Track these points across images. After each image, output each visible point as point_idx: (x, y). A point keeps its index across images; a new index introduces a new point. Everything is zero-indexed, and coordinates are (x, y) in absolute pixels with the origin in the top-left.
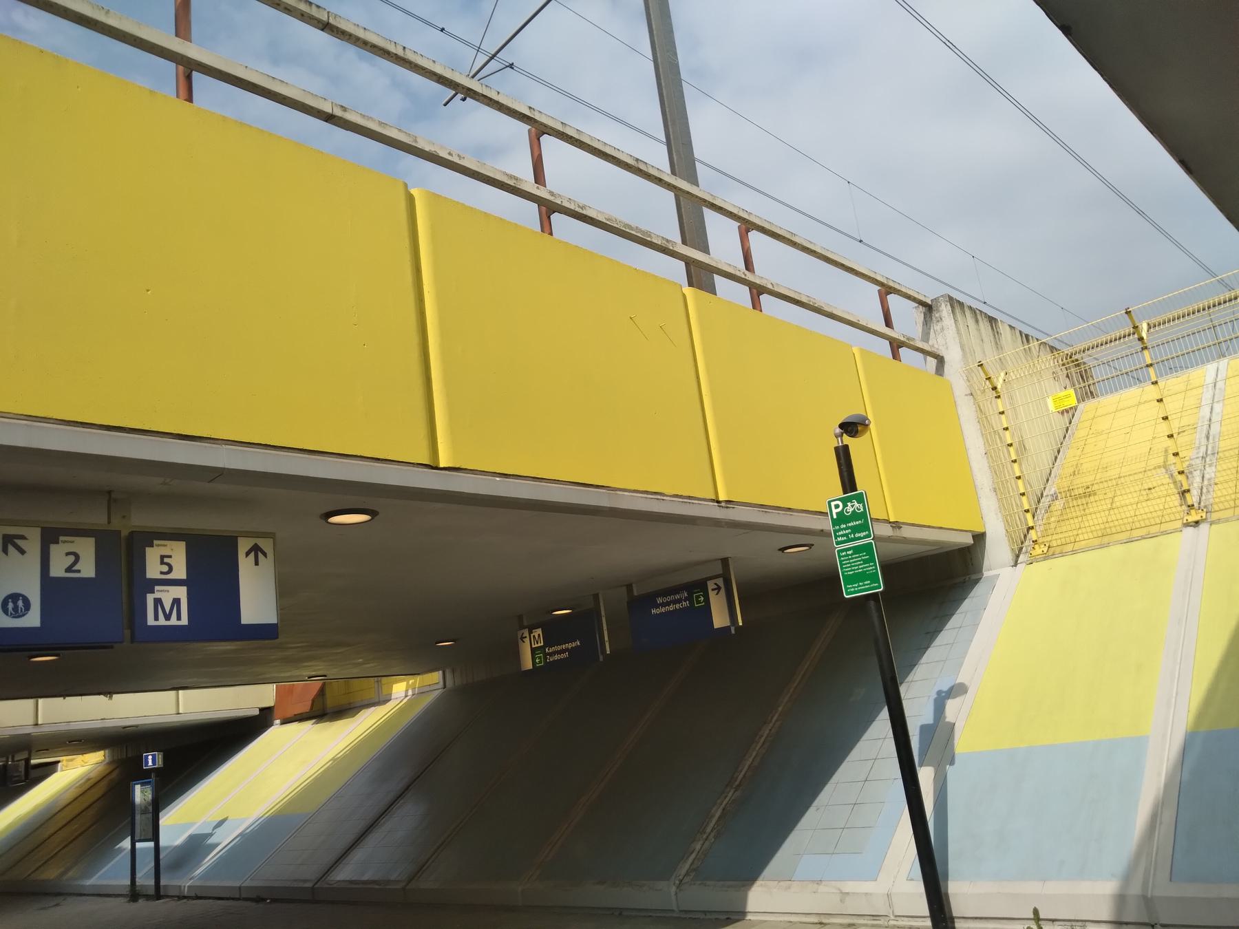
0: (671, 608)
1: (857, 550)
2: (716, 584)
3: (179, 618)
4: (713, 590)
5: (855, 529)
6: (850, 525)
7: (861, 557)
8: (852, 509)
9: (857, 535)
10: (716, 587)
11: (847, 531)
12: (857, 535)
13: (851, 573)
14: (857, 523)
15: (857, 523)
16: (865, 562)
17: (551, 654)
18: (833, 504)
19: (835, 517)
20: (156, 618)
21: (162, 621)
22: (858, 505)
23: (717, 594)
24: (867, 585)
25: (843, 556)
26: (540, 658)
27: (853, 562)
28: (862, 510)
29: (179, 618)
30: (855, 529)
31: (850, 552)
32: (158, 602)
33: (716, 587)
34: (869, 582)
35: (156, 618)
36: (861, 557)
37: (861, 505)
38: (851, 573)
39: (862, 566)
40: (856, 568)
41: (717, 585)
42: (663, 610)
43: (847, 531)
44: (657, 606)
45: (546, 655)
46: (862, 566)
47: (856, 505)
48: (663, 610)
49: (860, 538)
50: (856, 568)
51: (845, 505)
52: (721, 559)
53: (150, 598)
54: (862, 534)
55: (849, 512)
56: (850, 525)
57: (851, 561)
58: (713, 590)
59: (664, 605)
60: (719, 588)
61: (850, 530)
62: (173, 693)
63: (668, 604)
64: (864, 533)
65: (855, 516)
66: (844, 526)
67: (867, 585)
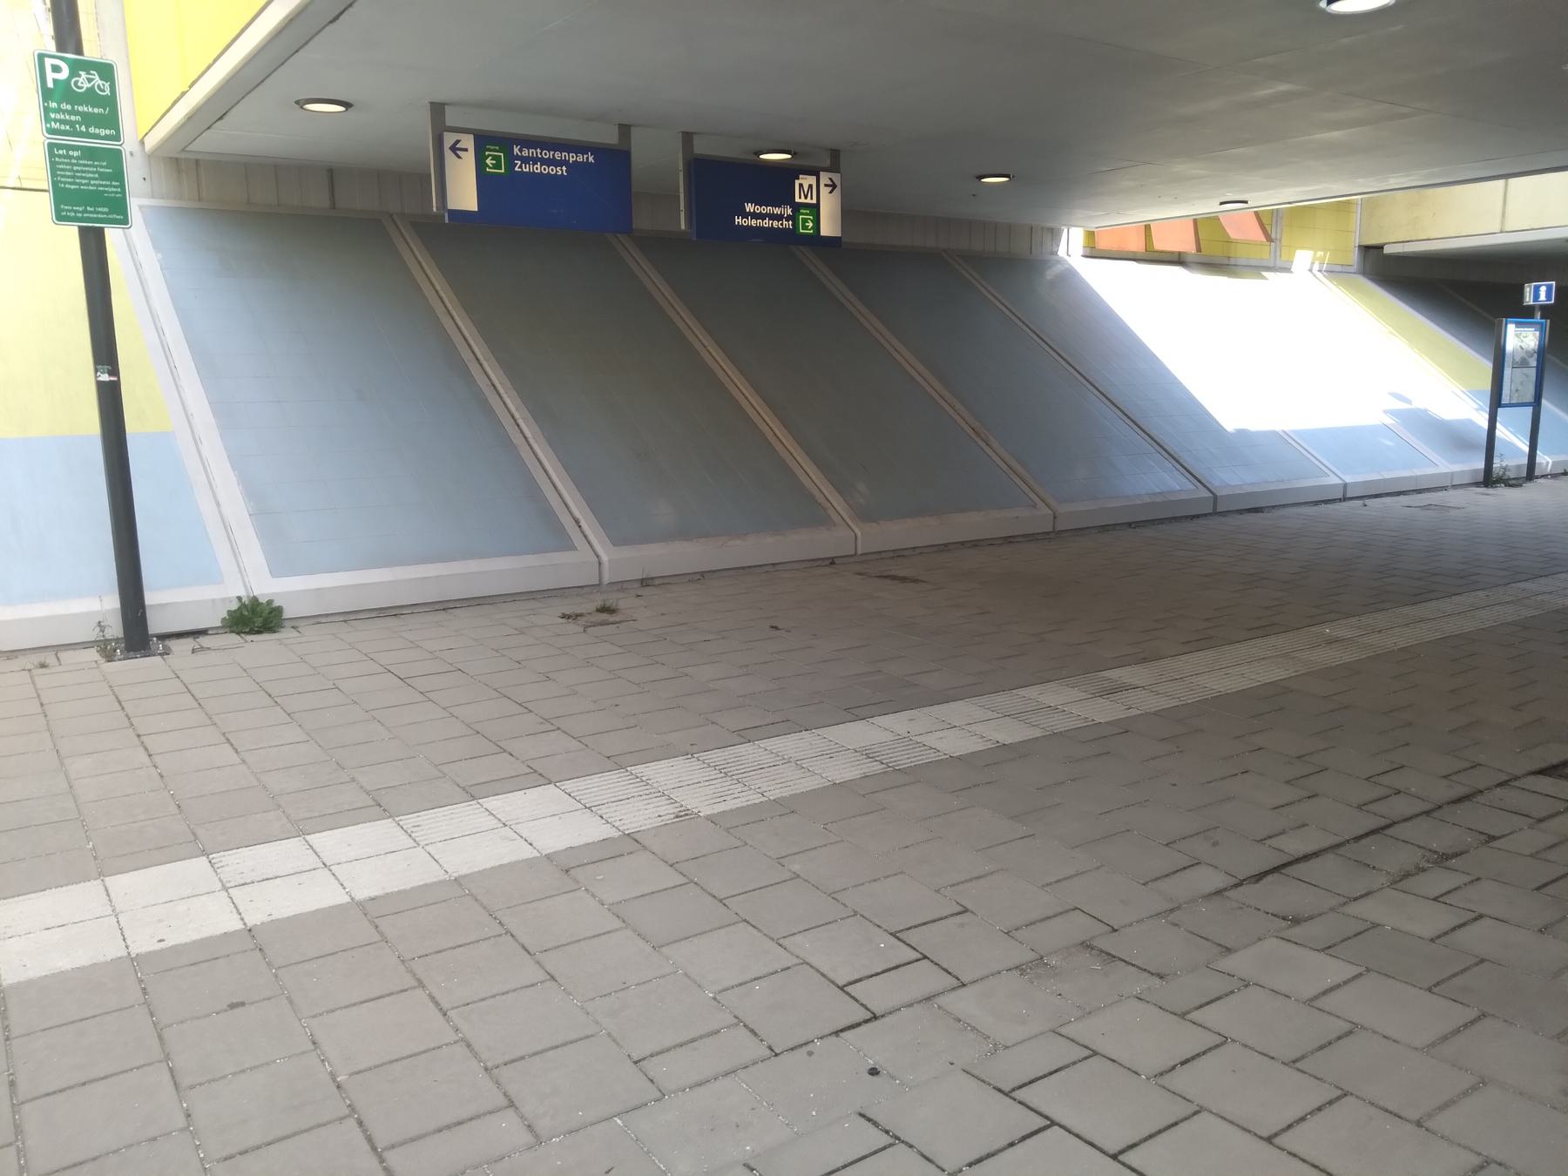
0: (766, 223)
1: (90, 153)
2: (830, 179)
3: (812, 199)
4: (826, 185)
5: (88, 119)
6: (80, 109)
7: (96, 166)
8: (89, 85)
9: (92, 130)
10: (830, 183)
11: (73, 118)
12: (92, 130)
13: (73, 187)
14: (96, 110)
15: (96, 110)
16: (102, 176)
17: (525, 160)
18: (48, 62)
19: (50, 84)
20: (800, 198)
21: (803, 200)
22: (100, 82)
23: (831, 192)
24: (103, 213)
25: (60, 156)
26: (805, 228)
27: (78, 171)
28: (108, 92)
29: (812, 199)
30: (88, 119)
31: (76, 154)
32: (801, 185)
33: (830, 183)
34: (106, 210)
35: (800, 198)
36: (96, 166)
37: (107, 85)
38: (73, 187)
39: (97, 182)
40: (84, 181)
41: (832, 181)
42: (754, 223)
43: (73, 118)
44: (745, 215)
45: (511, 159)
46: (97, 182)
47: (97, 81)
48: (754, 223)
49: (97, 136)
50: (84, 181)
51: (74, 73)
52: (831, 150)
53: (797, 183)
54: (103, 132)
55: (82, 88)
56: (80, 109)
57: (75, 168)
58: (826, 185)
59: (755, 216)
60: (834, 186)
61: (78, 118)
62: (1501, 183)
63: (762, 216)
64: (108, 132)
65: (91, 97)
66: (69, 107)
67: (103, 213)
